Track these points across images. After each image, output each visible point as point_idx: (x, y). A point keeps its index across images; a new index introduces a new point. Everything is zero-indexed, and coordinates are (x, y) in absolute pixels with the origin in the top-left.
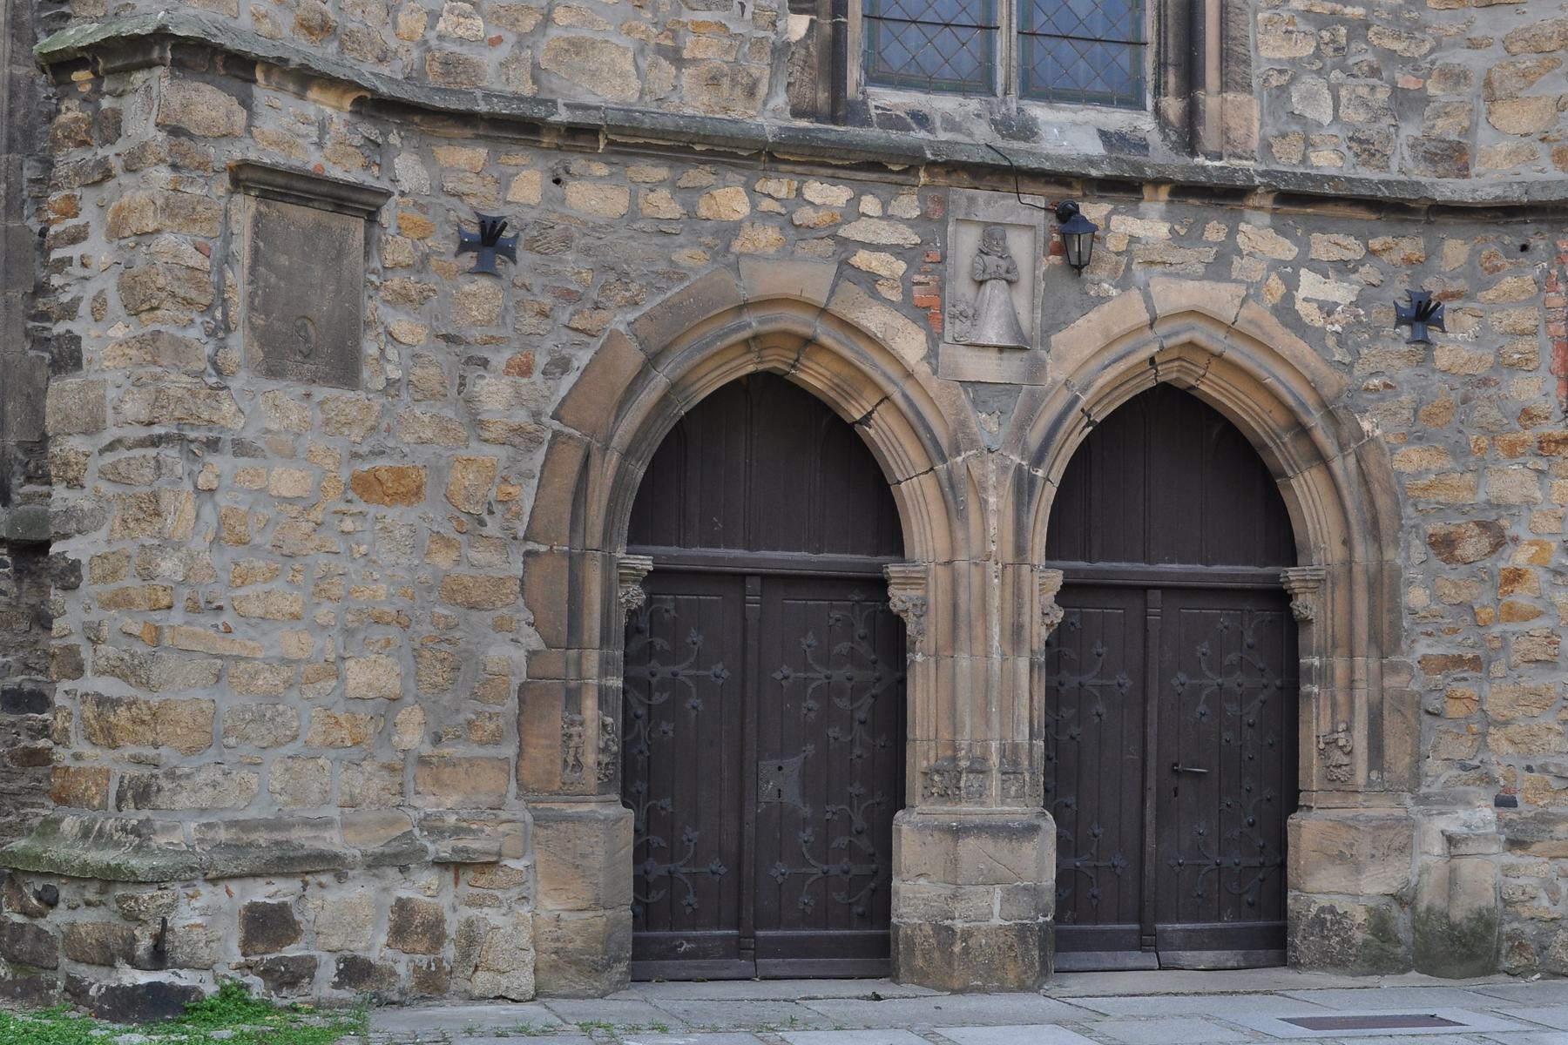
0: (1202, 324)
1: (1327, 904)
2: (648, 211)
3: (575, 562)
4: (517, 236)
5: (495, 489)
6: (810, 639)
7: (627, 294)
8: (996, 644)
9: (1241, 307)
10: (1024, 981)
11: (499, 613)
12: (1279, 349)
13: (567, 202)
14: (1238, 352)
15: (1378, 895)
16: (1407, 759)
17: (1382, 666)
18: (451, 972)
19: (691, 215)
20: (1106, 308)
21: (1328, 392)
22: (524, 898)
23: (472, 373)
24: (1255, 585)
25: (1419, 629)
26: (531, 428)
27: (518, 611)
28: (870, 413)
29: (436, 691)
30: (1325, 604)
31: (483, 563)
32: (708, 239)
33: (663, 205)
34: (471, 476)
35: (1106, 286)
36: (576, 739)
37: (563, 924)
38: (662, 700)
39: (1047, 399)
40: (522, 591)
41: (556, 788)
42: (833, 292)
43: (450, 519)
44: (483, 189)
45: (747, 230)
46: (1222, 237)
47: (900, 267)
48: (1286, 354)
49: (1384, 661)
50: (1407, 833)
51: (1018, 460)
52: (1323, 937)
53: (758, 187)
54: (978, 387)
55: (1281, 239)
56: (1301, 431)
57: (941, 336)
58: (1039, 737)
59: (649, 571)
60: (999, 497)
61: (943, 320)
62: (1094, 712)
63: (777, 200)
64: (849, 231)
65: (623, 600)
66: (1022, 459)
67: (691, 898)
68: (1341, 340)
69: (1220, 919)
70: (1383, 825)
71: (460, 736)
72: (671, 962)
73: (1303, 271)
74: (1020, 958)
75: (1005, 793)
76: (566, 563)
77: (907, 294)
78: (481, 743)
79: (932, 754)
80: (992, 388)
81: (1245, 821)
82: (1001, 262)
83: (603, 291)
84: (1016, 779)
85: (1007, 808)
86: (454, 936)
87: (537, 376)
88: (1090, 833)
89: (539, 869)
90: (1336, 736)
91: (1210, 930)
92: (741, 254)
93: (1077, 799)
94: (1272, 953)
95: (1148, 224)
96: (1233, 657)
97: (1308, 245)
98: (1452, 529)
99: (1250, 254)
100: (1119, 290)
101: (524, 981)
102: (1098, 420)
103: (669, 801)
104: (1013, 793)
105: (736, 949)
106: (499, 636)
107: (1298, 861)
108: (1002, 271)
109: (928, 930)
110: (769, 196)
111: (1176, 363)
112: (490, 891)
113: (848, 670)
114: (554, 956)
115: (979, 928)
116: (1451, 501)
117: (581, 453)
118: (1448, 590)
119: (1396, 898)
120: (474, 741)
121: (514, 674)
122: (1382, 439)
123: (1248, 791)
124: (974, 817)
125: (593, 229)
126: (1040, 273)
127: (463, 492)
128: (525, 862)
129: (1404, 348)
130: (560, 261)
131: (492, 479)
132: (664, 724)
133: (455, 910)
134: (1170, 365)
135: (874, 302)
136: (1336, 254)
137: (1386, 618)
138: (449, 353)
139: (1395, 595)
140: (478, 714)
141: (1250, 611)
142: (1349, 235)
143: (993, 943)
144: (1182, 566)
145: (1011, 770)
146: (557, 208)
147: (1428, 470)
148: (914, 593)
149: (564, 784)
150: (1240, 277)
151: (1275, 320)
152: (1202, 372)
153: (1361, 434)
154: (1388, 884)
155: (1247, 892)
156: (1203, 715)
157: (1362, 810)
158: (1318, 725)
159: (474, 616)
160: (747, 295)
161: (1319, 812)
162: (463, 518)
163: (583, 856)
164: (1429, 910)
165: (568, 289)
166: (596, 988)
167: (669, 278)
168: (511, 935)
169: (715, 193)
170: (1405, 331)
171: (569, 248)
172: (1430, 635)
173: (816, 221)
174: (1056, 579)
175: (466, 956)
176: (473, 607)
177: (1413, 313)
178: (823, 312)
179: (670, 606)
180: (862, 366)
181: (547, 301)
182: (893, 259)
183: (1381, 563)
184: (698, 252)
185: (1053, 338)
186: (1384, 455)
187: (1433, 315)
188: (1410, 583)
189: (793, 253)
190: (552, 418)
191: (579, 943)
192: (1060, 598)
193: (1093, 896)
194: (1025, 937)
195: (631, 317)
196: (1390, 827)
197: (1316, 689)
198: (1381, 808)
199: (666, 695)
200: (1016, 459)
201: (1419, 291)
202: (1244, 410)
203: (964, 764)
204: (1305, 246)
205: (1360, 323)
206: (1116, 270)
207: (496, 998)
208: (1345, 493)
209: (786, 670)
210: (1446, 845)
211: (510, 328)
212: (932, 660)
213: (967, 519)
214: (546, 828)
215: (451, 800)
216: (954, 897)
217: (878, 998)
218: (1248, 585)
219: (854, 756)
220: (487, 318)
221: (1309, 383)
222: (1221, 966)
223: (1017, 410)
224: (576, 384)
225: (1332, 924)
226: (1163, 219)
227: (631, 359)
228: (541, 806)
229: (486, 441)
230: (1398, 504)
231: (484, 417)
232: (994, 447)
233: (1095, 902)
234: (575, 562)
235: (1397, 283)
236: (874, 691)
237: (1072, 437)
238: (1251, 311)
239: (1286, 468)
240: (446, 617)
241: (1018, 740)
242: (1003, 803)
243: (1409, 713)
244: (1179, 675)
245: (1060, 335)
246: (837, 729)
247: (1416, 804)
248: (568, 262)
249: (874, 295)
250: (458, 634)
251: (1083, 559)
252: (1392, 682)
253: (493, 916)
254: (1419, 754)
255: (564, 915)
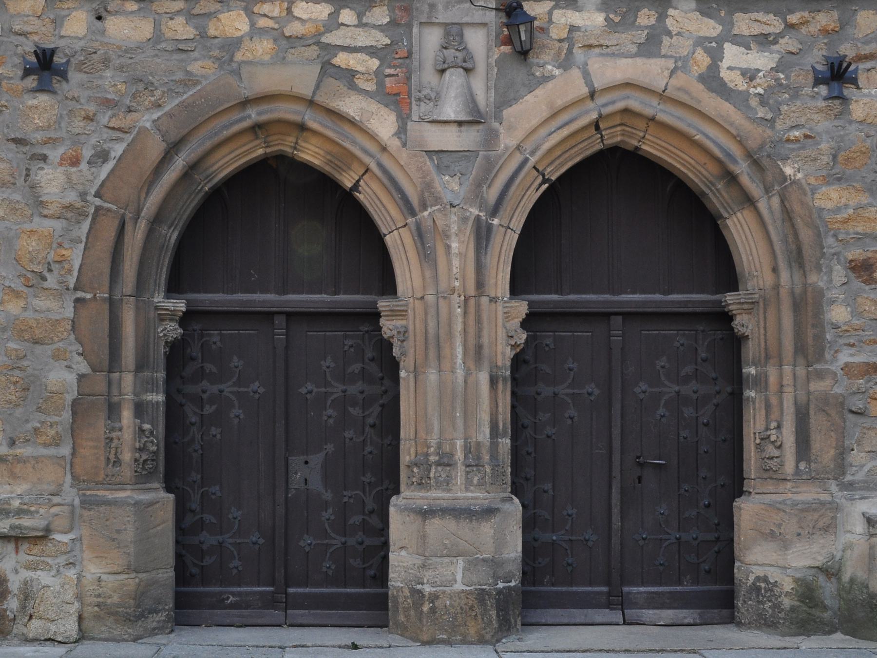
0: (638, 94)
1: (762, 575)
2: (169, 34)
3: (114, 307)
4: (68, 61)
5: (52, 252)
6: (329, 362)
7: (153, 99)
8: (459, 361)
9: (670, 77)
10: (483, 636)
11: (55, 346)
12: (706, 110)
13: (107, 33)
14: (668, 115)
15: (805, 567)
16: (832, 452)
17: (808, 373)
18: (14, 619)
19: (203, 35)
20: (550, 85)
21: (752, 144)
22: (71, 563)
23: (35, 166)
24: (706, 310)
25: (842, 341)
26: (79, 204)
27: (71, 344)
28: (358, 181)
29: (11, 406)
30: (758, 322)
31: (44, 308)
32: (216, 53)
33: (180, 29)
34: (34, 244)
35: (549, 67)
36: (116, 441)
37: (103, 584)
38: (211, 411)
39: (500, 163)
40: (73, 329)
41: (101, 479)
42: (317, 87)
43: (19, 276)
44: (43, 28)
45: (247, 43)
46: (653, 21)
47: (374, 63)
48: (712, 114)
49: (810, 369)
50: (831, 515)
51: (477, 212)
52: (758, 602)
53: (256, 10)
54: (441, 155)
55: (706, 20)
56: (731, 178)
57: (409, 116)
58: (504, 435)
59: (182, 312)
60: (460, 242)
61: (411, 103)
62: (567, 415)
63: (271, 18)
64: (333, 38)
65: (161, 335)
66: (480, 211)
67: (236, 563)
68: (763, 100)
69: (680, 583)
70: (808, 508)
71: (29, 440)
72: (219, 611)
73: (727, 45)
74: (479, 617)
75: (468, 483)
76: (106, 306)
77: (380, 84)
78: (46, 445)
79: (413, 450)
80: (456, 155)
81: (701, 504)
82: (458, 54)
83: (135, 98)
84: (478, 470)
85: (470, 494)
86: (16, 592)
87: (84, 166)
88: (565, 513)
89: (85, 542)
90: (769, 433)
91: (670, 593)
92: (243, 62)
93: (553, 486)
94: (725, 612)
95: (585, 15)
96: (688, 369)
97: (732, 24)
98: (870, 255)
99: (679, 34)
100: (561, 70)
101: (70, 627)
102: (553, 178)
103: (217, 488)
104: (475, 481)
105: (270, 602)
106: (57, 364)
107: (739, 537)
108: (459, 61)
109: (407, 593)
110: (265, 15)
111: (619, 128)
112: (42, 558)
113: (359, 385)
114: (96, 608)
115: (444, 592)
116: (869, 231)
117: (116, 223)
118: (868, 306)
119: (824, 570)
120: (40, 444)
121: (68, 393)
122: (803, 182)
123: (704, 478)
124: (442, 502)
125: (126, 51)
126: (492, 61)
127: (28, 256)
128: (72, 536)
129: (821, 104)
130: (101, 77)
131: (50, 245)
132: (213, 429)
133: (17, 572)
134: (615, 130)
135: (352, 92)
136: (756, 29)
137: (810, 332)
138: (18, 152)
139: (818, 312)
140: (43, 423)
141: (703, 331)
142: (768, 13)
143: (456, 604)
144: (643, 296)
145: (473, 464)
146: (99, 38)
147: (846, 206)
148: (399, 323)
149: (107, 476)
150: (670, 53)
151: (701, 87)
152: (642, 134)
153: (784, 178)
154: (814, 559)
155: (704, 561)
156: (662, 416)
157: (790, 495)
158: (754, 423)
159: (39, 349)
160: (247, 93)
161: (757, 496)
162: (29, 275)
163: (118, 532)
164: (852, 581)
165: (106, 99)
166: (130, 634)
167: (185, 84)
168: (59, 592)
169: (221, 16)
170: (823, 90)
171: (108, 67)
172: (853, 345)
173: (304, 32)
174: (521, 308)
175: (23, 607)
176: (36, 342)
177: (829, 74)
178: (311, 103)
179: (216, 339)
180: (344, 144)
181: (92, 108)
182: (368, 58)
183: (805, 285)
184: (208, 63)
185: (505, 112)
186: (805, 195)
187: (847, 75)
188: (833, 302)
189: (284, 58)
190: (95, 196)
191: (116, 599)
192: (525, 325)
193: (569, 565)
194: (484, 600)
195: (155, 116)
196: (815, 510)
197: (753, 394)
198: (808, 494)
199: (214, 407)
200: (475, 211)
201: (836, 55)
202: (684, 165)
203: (433, 458)
204: (728, 24)
205: (781, 85)
206: (558, 54)
207: (46, 640)
208: (771, 229)
209: (310, 386)
210: (866, 526)
211: (64, 131)
212: (412, 375)
213: (436, 261)
214: (90, 510)
215: (21, 488)
216: (424, 566)
217: (355, 647)
218: (698, 310)
219: (366, 453)
220: (46, 124)
221: (735, 137)
222: (679, 622)
223: (474, 173)
224: (113, 171)
225: (766, 591)
226: (599, 10)
227: (155, 148)
228: (88, 493)
229: (45, 216)
230: (819, 235)
231: (44, 199)
232: (456, 202)
233: (569, 569)
234: (114, 307)
235: (815, 51)
236: (381, 402)
237: (529, 193)
238: (680, 80)
239: (722, 211)
240: (16, 350)
241: (480, 438)
242: (467, 490)
243: (833, 413)
244: (641, 384)
245: (510, 110)
246: (352, 432)
247: (840, 490)
248: (107, 77)
249: (353, 87)
250: (25, 363)
251: (556, 293)
252: (816, 386)
253: (44, 577)
254: (843, 446)
255: (104, 577)
